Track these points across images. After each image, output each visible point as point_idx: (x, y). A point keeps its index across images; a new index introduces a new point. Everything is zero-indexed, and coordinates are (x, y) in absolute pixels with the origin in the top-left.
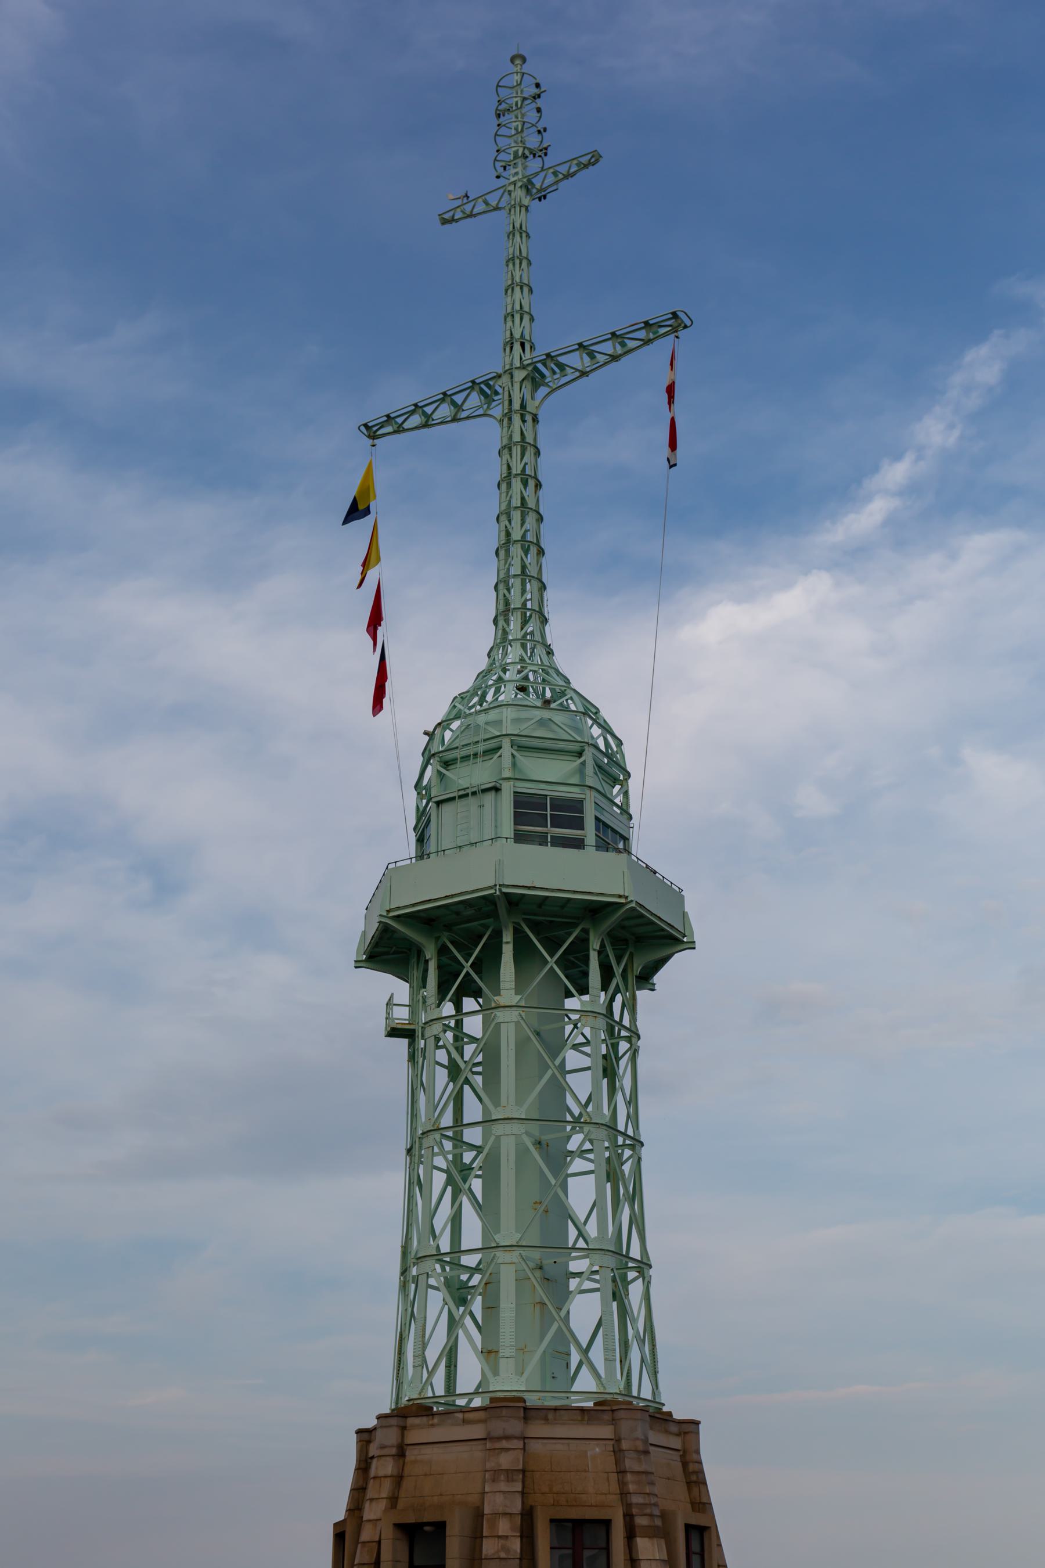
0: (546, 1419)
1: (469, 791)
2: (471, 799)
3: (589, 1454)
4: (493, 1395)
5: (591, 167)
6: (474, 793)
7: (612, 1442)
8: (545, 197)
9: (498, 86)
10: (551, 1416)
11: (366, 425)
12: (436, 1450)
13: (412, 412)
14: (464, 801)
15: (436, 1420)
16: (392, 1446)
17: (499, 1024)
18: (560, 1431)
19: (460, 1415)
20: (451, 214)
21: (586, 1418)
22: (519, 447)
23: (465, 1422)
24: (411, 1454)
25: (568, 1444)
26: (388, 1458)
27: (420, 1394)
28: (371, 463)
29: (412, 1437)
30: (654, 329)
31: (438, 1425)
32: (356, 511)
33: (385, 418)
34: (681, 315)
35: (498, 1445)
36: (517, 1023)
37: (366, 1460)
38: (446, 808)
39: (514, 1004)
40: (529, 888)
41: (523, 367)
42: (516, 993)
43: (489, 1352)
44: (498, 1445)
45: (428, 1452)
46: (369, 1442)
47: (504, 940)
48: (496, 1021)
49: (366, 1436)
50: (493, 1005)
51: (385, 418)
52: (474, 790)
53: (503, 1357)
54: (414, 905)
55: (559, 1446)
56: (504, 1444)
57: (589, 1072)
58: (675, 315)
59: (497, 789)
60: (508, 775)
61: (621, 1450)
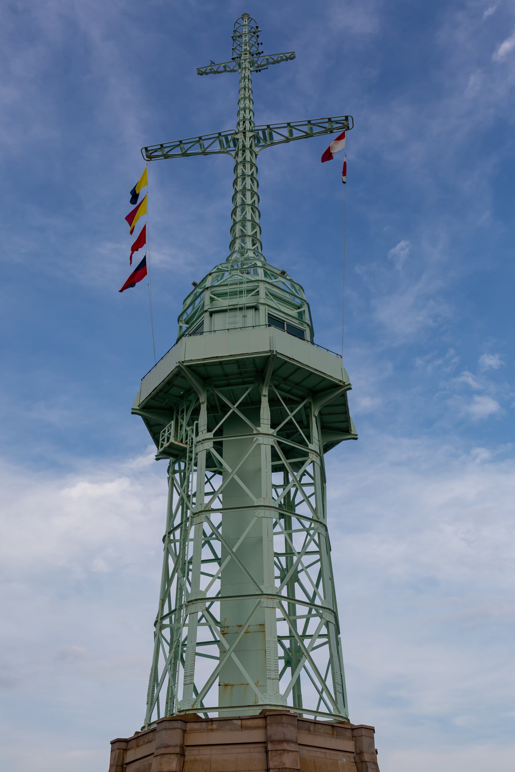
0: (309, 730)
2: (238, 313)
3: (339, 762)
4: (264, 708)
6: (241, 309)
7: (352, 755)
8: (260, 71)
10: (312, 727)
11: (146, 149)
12: (215, 751)
13: (177, 146)
14: (232, 314)
15: (215, 726)
16: (176, 746)
17: (259, 445)
18: (319, 741)
19: (239, 722)
22: (249, 165)
23: (242, 728)
24: (190, 754)
25: (325, 753)
26: (173, 756)
27: (193, 706)
29: (193, 739)
31: (217, 730)
33: (159, 147)
34: (349, 118)
35: (279, 747)
36: (272, 447)
37: (122, 766)
38: (216, 316)
40: (290, 358)
42: (271, 427)
43: (226, 685)
44: (279, 747)
45: (206, 753)
46: (125, 750)
47: (264, 394)
49: (123, 745)
50: (255, 432)
51: (159, 147)
52: (241, 306)
53: (270, 678)
55: (319, 754)
56: (286, 746)
58: (347, 118)
61: (363, 762)
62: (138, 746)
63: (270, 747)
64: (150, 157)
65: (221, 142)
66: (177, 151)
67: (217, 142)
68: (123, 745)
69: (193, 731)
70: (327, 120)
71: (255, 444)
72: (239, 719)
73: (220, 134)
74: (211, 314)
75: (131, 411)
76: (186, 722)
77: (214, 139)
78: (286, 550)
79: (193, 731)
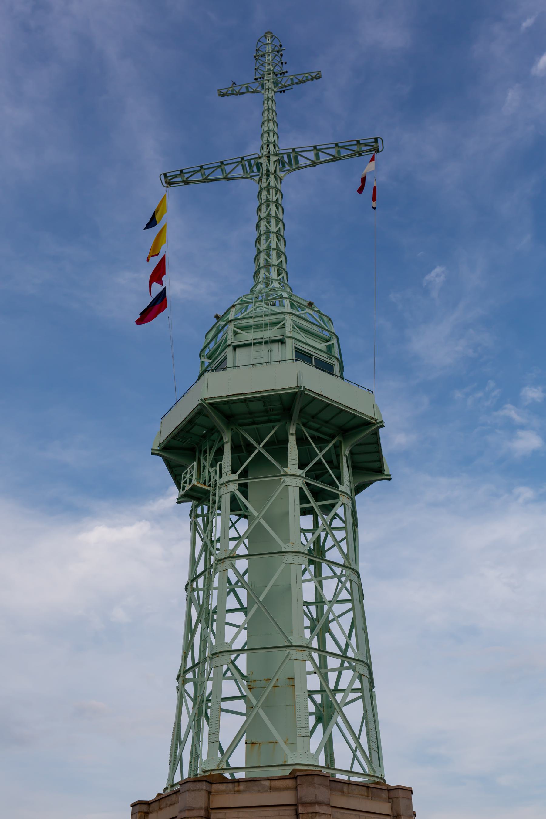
0: (342, 791)
1: (263, 340)
2: (263, 347)
4: (294, 767)
5: (315, 80)
6: (266, 343)
8: (284, 91)
9: (259, 41)
10: (345, 788)
11: (165, 175)
14: (257, 348)
15: (242, 787)
16: (201, 809)
18: (353, 803)
19: (267, 783)
20: (226, 91)
21: (370, 794)
22: (274, 190)
23: (271, 788)
28: (165, 196)
29: (218, 801)
30: (361, 146)
31: (244, 791)
32: (152, 223)
33: (179, 172)
34: (379, 140)
36: (301, 489)
38: (240, 351)
39: (299, 474)
40: (319, 395)
41: (276, 155)
43: (253, 743)
44: (310, 810)
47: (291, 432)
48: (285, 484)
49: (144, 808)
50: (282, 473)
51: (179, 172)
52: (266, 339)
54: (227, 396)
56: (317, 809)
57: (228, 608)
59: (282, 342)
60: (289, 335)
62: (160, 809)
63: (301, 809)
64: (169, 184)
65: (243, 167)
66: (218, 174)
67: (240, 167)
68: (144, 808)
69: (218, 792)
70: (355, 142)
71: (283, 486)
72: (268, 779)
73: (242, 158)
74: (235, 348)
75: (150, 451)
76: (211, 783)
77: (236, 164)
78: (316, 599)
79: (218, 792)
